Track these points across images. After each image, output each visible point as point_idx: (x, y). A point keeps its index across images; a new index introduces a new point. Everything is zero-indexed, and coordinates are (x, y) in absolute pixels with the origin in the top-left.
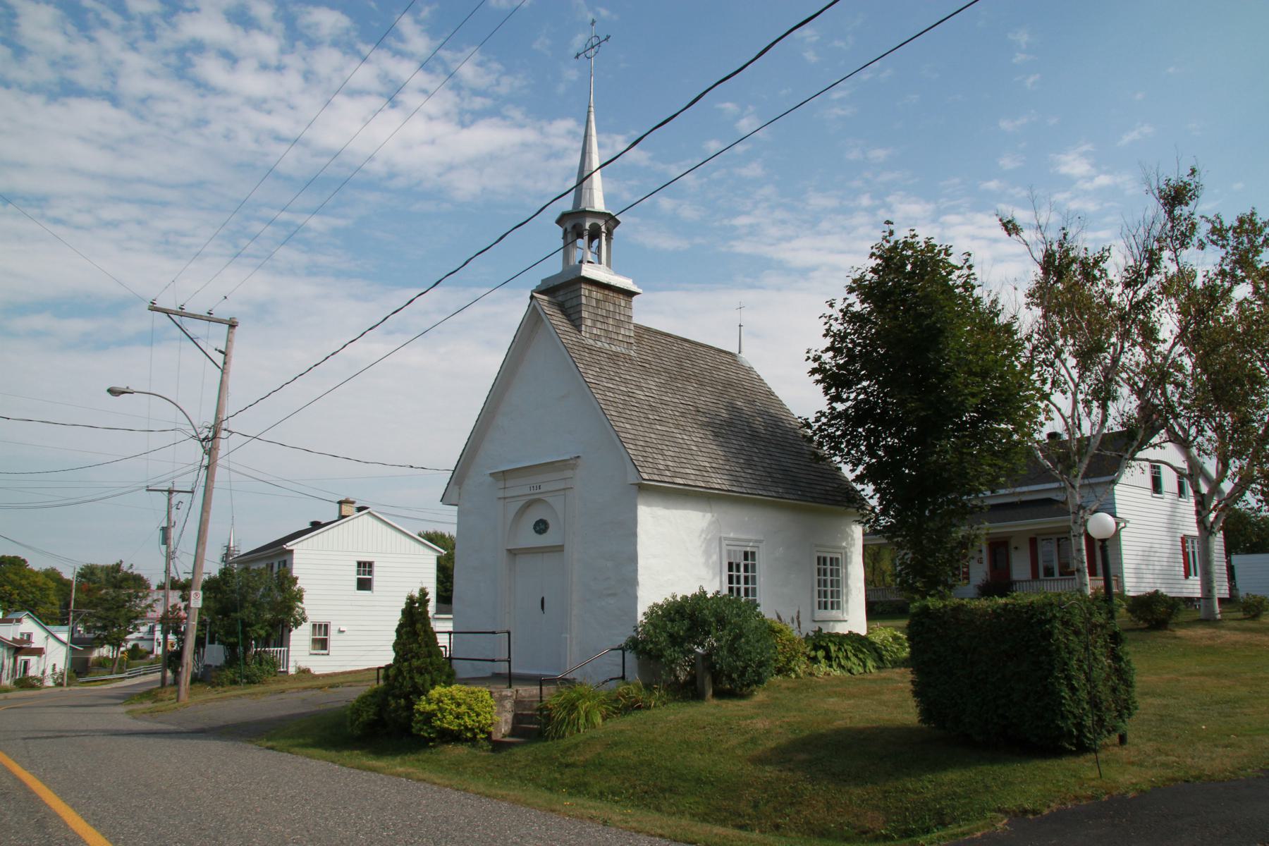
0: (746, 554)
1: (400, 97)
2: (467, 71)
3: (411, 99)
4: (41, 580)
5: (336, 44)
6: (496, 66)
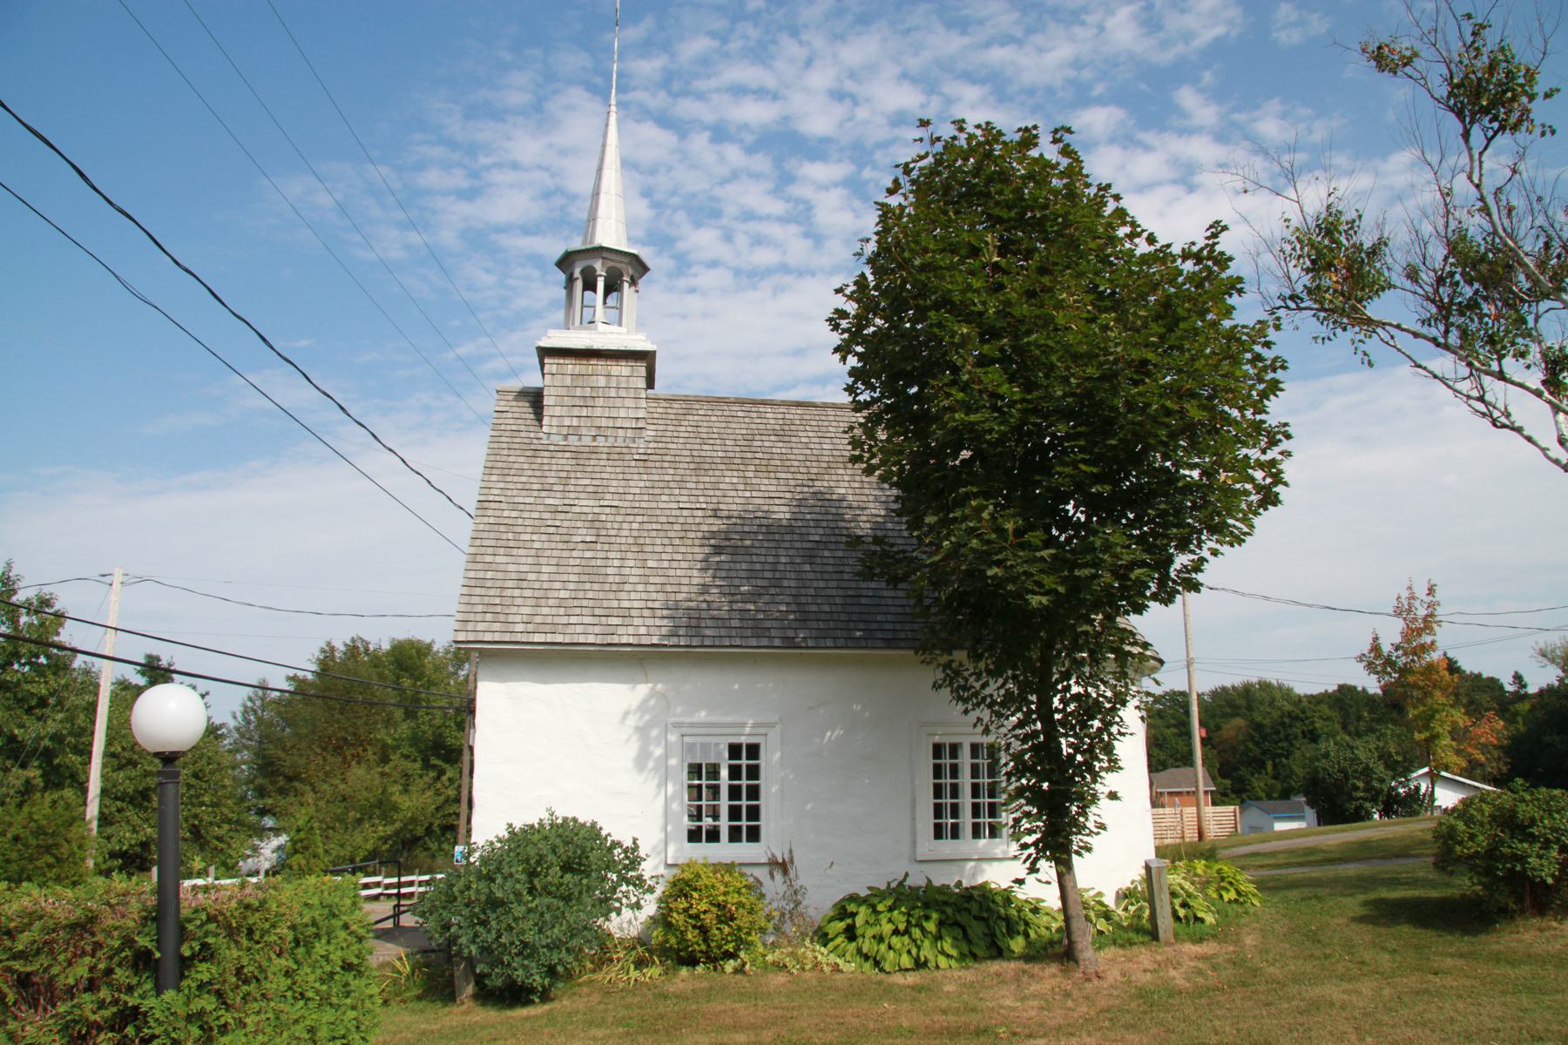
0: (735, 751)
1: (1198, 179)
2: (1270, 128)
3: (1207, 179)
4: (1305, 703)
5: (1112, 141)
6: (1305, 112)
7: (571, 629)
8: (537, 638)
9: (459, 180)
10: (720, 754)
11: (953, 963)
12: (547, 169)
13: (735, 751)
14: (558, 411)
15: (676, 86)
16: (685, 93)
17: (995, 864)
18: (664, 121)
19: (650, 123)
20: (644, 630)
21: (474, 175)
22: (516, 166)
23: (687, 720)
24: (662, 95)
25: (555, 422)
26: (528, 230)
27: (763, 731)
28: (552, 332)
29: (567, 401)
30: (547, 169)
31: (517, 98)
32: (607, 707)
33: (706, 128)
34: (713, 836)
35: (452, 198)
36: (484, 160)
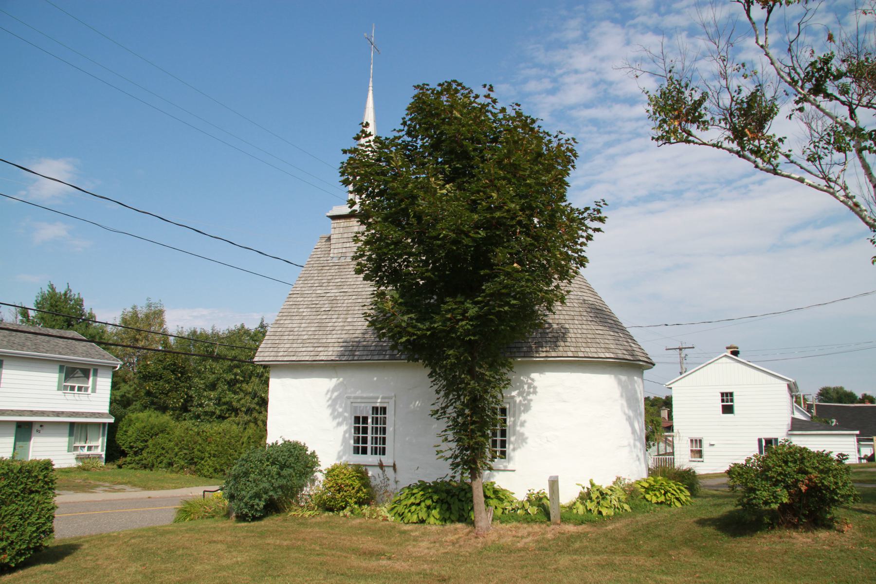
7: (300, 354)
8: (286, 359)
9: (547, 84)
10: (368, 412)
11: (437, 522)
12: (594, 70)
13: (375, 410)
14: (337, 246)
15: (663, 9)
16: (669, 12)
17: (501, 473)
18: (658, 31)
19: (650, 33)
20: (330, 353)
21: (555, 80)
22: (576, 72)
23: (353, 395)
24: (655, 15)
25: (336, 251)
26: (587, 106)
27: (386, 400)
28: (334, 208)
29: (342, 240)
30: (594, 70)
31: (572, 35)
32: (321, 386)
33: (684, 30)
34: (364, 451)
35: (544, 95)
36: (559, 72)
